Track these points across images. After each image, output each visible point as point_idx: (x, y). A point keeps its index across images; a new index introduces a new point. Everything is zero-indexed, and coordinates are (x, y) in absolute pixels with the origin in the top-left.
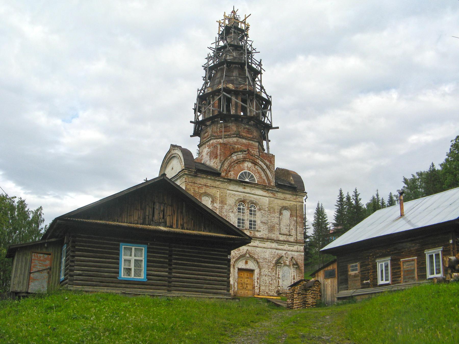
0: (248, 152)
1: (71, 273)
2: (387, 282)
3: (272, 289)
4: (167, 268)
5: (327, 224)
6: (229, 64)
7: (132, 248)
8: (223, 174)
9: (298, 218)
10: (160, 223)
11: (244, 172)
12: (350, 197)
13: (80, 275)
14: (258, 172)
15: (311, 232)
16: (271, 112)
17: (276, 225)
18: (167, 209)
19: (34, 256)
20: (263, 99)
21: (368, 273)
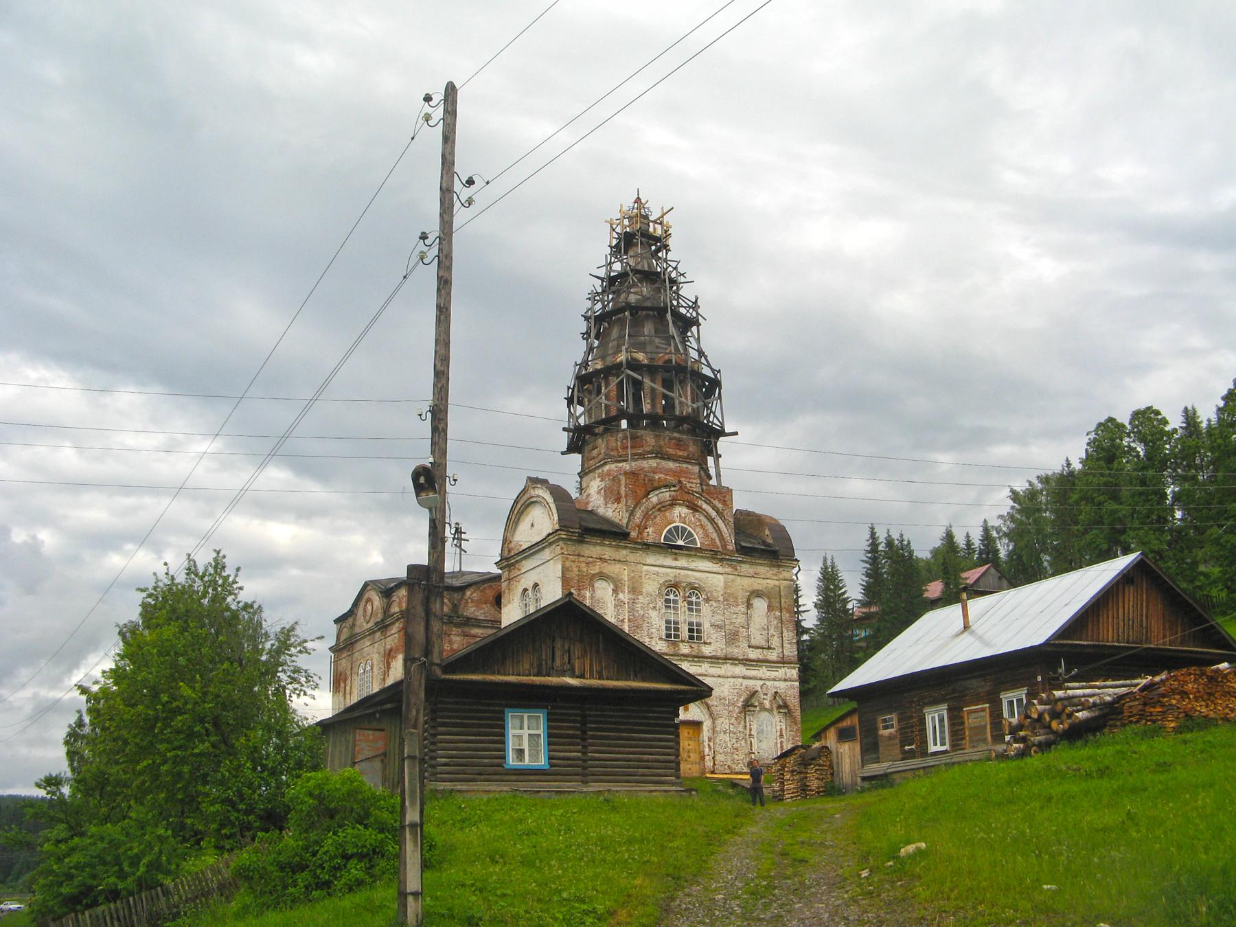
1: (433, 762)
2: (944, 748)
3: (738, 758)
4: (579, 745)
5: (846, 601)
6: (635, 310)
7: (523, 716)
8: (633, 534)
9: (784, 612)
12: (893, 540)
13: (446, 765)
14: (702, 526)
15: (810, 619)
17: (741, 630)
18: (574, 649)
19: (359, 734)
20: (707, 378)
21: (912, 732)
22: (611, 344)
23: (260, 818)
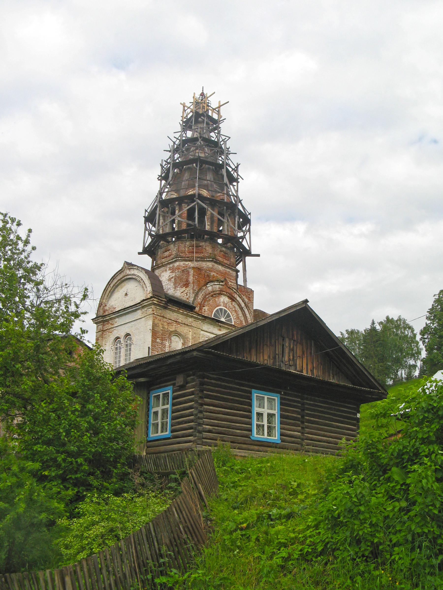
0: (226, 284)
1: (200, 428)
10: (290, 366)
11: (220, 309)
13: (210, 431)
14: (236, 311)
16: (250, 234)
22: (183, 183)
23: (89, 461)
